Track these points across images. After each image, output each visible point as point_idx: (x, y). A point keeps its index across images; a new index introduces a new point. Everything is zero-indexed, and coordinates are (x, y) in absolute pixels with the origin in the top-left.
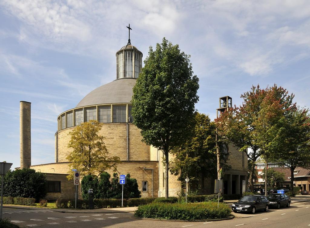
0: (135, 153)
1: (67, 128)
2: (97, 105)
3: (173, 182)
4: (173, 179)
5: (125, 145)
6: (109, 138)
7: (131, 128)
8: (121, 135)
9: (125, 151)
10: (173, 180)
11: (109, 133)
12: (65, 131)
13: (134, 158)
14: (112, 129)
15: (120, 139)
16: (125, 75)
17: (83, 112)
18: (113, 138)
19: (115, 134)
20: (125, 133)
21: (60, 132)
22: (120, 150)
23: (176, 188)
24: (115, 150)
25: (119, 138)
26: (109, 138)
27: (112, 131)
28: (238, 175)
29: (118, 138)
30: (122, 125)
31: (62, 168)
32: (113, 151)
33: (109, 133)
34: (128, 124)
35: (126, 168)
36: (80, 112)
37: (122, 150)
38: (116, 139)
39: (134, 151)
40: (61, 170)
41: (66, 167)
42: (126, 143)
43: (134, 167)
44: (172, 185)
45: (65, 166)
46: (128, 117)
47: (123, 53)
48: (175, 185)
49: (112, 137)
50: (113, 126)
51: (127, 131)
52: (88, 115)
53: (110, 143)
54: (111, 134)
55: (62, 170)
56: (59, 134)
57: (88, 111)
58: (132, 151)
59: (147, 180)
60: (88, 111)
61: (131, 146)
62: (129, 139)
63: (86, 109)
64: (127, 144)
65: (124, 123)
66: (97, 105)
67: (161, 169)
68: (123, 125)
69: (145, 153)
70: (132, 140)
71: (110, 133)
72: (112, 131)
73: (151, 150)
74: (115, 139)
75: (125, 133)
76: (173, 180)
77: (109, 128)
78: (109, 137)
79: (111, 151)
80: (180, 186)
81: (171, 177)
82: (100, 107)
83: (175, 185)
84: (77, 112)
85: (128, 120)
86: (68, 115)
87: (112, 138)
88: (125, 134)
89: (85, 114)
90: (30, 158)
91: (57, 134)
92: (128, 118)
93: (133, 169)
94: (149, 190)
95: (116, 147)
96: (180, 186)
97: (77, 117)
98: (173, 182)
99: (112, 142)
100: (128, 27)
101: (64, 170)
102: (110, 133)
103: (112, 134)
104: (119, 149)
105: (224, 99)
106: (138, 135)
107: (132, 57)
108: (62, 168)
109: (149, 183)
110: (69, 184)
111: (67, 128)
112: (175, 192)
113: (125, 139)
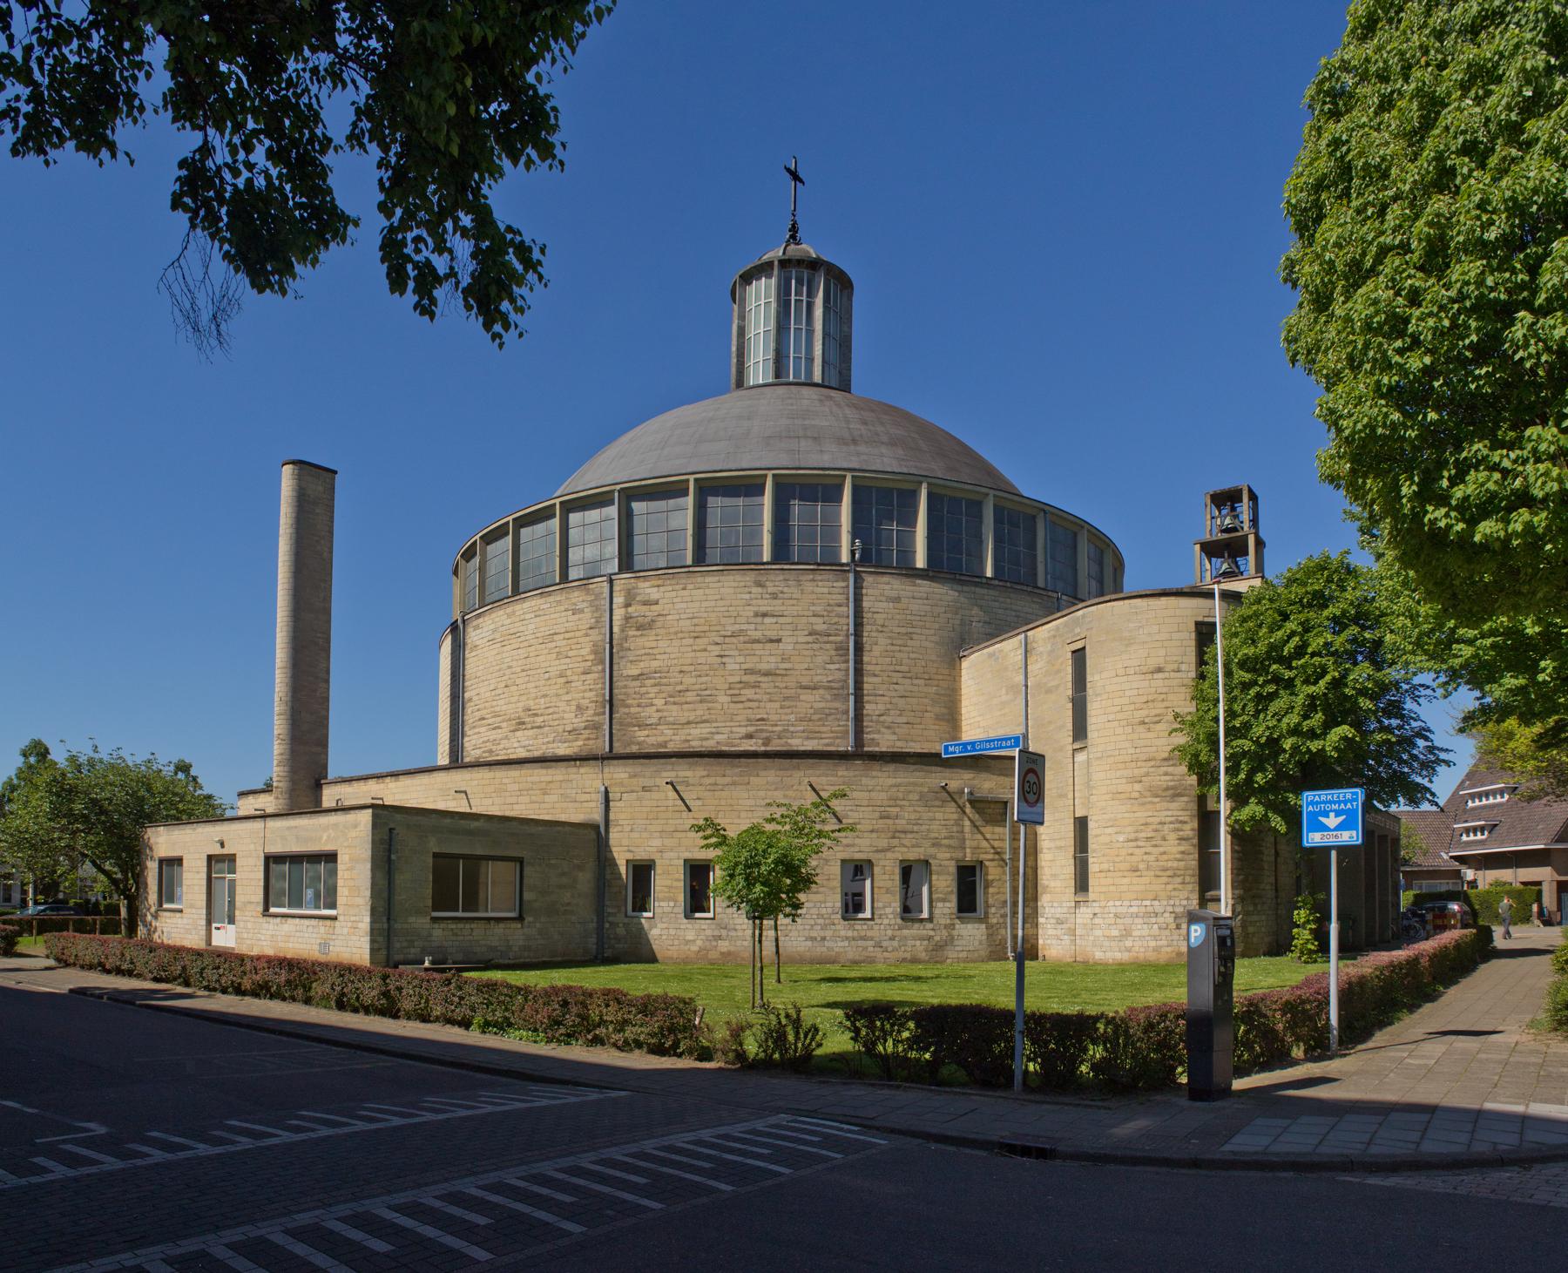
0: (889, 719)
1: (516, 591)
2: (692, 478)
3: (1148, 869)
4: (1149, 849)
5: (839, 675)
6: (758, 641)
7: (870, 592)
8: (821, 627)
9: (837, 705)
10: (1152, 858)
11: (756, 615)
12: (509, 610)
13: (882, 740)
14: (774, 596)
15: (815, 646)
16: (780, 370)
17: (612, 511)
18: (779, 641)
19: (789, 620)
20: (838, 616)
21: (479, 616)
22: (812, 701)
23: (1170, 898)
24: (787, 703)
25: (810, 639)
26: (758, 641)
27: (775, 605)
28: (333, 906)
29: (801, 639)
30: (826, 576)
31: (516, 787)
32: (777, 705)
33: (756, 615)
34: (856, 572)
35: (873, 794)
36: (593, 515)
37: (823, 699)
38: (790, 647)
39: (881, 707)
40: (510, 800)
41: (543, 785)
42: (843, 666)
43: (915, 784)
44: (1146, 880)
45: (535, 779)
46: (855, 534)
47: (769, 276)
48: (1165, 880)
49: (773, 634)
50: (775, 580)
51: (851, 605)
52: (639, 525)
53: (764, 667)
54: (767, 620)
55: (513, 800)
56: (477, 627)
57: (637, 506)
58: (873, 706)
59: (982, 857)
60: (637, 506)
61: (869, 683)
62: (859, 649)
63: (631, 495)
64: (847, 670)
65: (829, 562)
66: (692, 478)
67: (1061, 796)
68: (831, 576)
69: (938, 718)
70: (877, 651)
71: (764, 615)
72: (775, 605)
73: (964, 703)
74: (787, 646)
75: (838, 616)
76: (1152, 858)
77: (760, 590)
78: (757, 635)
79: (769, 705)
80: (1190, 887)
81: (1136, 840)
82: (709, 488)
83: (1165, 880)
84: (574, 518)
85: (853, 553)
86: (525, 532)
87: (772, 641)
88: (844, 621)
89: (626, 518)
90: (323, 743)
91: (457, 631)
92: (853, 543)
93: (911, 797)
94: (993, 910)
95: (793, 685)
96: (1190, 887)
97: (574, 534)
98: (1148, 869)
99: (773, 659)
100: (788, 170)
101: (525, 799)
102: (764, 615)
103: (774, 620)
104: (807, 696)
105: (1226, 499)
106: (903, 630)
107: (811, 294)
108: (516, 787)
109: (991, 870)
110: (563, 874)
111: (516, 591)
112: (1160, 920)
113: (841, 649)
